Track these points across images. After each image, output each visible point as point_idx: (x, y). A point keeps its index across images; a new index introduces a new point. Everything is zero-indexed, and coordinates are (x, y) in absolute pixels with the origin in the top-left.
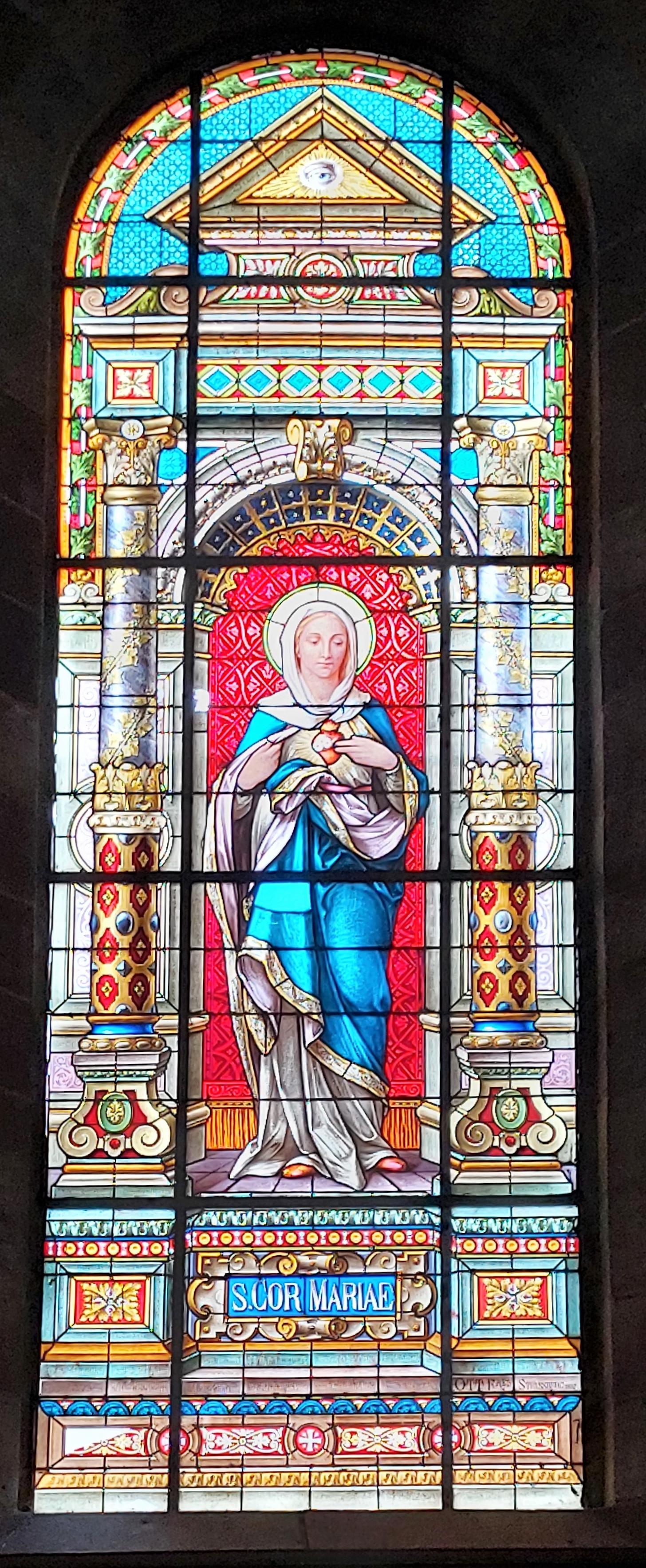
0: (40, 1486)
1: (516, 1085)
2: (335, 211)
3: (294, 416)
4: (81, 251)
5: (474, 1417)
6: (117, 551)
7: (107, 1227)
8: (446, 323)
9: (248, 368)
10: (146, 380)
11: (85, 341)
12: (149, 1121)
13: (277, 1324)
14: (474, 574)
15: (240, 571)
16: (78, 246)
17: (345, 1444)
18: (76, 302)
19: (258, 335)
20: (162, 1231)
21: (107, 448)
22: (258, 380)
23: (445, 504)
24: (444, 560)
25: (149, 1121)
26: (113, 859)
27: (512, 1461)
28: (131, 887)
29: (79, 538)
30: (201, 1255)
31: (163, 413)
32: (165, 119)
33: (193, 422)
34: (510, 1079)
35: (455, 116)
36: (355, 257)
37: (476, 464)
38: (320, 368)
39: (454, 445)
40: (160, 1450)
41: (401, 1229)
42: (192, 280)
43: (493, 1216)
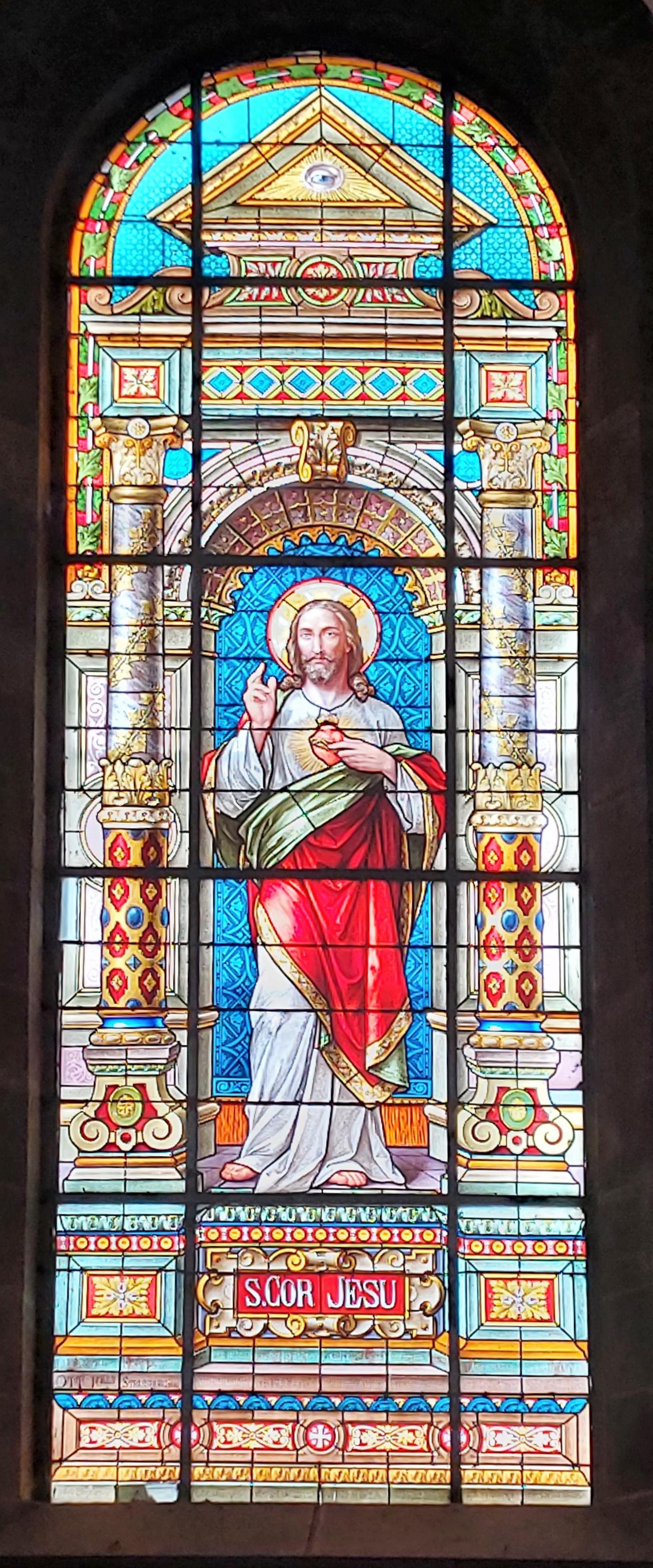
0: (55, 1478)
1: (523, 1084)
2: (273, 213)
3: (298, 418)
4: (87, 251)
5: (348, 1416)
6: (123, 549)
7: (118, 1222)
8: (448, 326)
9: (211, 370)
10: (519, 383)
11: (91, 339)
12: (160, 1115)
13: (286, 1320)
14: (478, 577)
15: (245, 570)
16: (82, 247)
17: (353, 1444)
18: (83, 300)
19: (385, 338)
20: (173, 1226)
21: (113, 446)
22: (263, 382)
23: (449, 507)
24: (450, 562)
25: (160, 1115)
26: (123, 855)
27: (384, 1461)
28: (515, 885)
29: (86, 535)
30: (210, 1251)
31: (169, 413)
32: (166, 121)
33: (195, 421)
34: (126, 1076)
35: (456, 121)
36: (356, 259)
37: (484, 467)
38: (323, 369)
39: (457, 449)
40: (173, 1442)
41: (346, 1226)
42: (197, 281)
43: (500, 1218)
